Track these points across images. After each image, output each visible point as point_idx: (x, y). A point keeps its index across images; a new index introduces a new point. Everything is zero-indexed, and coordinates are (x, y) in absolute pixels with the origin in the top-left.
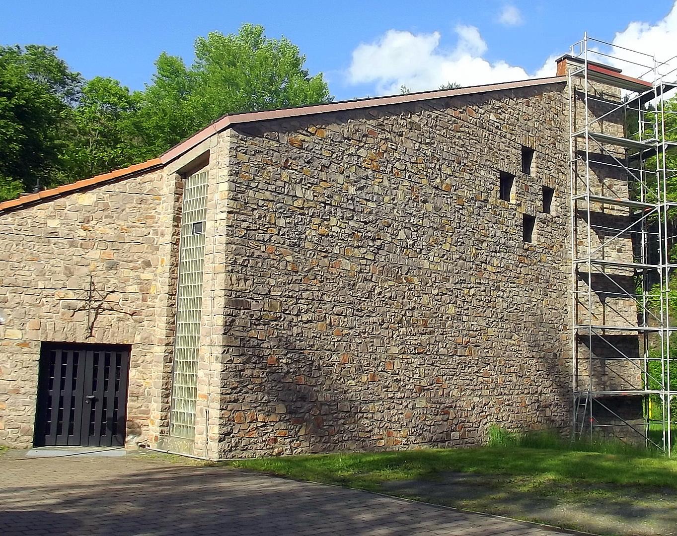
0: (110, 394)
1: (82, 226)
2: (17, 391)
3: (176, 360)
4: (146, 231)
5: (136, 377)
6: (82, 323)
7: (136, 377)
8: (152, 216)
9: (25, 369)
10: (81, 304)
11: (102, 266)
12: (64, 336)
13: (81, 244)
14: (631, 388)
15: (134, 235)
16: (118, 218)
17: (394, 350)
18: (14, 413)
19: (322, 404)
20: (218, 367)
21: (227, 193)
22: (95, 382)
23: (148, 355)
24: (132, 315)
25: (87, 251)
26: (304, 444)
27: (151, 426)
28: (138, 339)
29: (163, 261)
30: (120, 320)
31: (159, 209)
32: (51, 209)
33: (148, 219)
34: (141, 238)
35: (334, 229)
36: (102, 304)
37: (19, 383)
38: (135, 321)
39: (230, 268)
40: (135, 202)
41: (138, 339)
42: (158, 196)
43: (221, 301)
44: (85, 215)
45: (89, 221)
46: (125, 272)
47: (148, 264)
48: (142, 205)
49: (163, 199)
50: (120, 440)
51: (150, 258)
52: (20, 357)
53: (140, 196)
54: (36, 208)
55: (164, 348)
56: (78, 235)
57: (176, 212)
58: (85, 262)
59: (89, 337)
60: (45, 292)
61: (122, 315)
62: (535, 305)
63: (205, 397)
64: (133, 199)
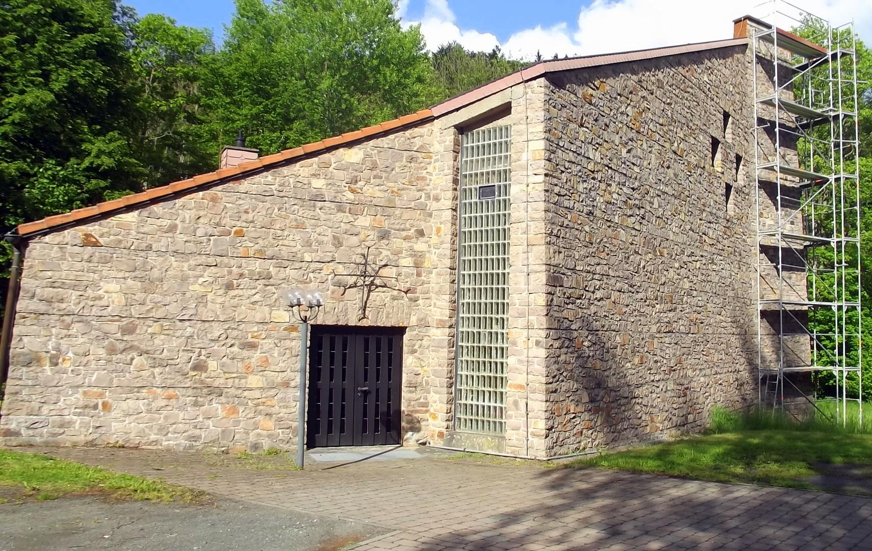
0: (383, 383)
1: (349, 187)
2: (286, 384)
3: (460, 344)
4: (418, 194)
5: (413, 365)
6: (354, 302)
7: (413, 365)
8: (423, 177)
9: (294, 358)
10: (351, 281)
11: (373, 235)
12: (335, 318)
13: (350, 209)
14: (803, 364)
15: (405, 198)
16: (387, 178)
18: (284, 410)
19: (611, 390)
20: (542, 353)
21: (543, 152)
22: (366, 371)
23: (426, 338)
24: (406, 293)
25: (356, 217)
26: (601, 435)
28: (414, 320)
29: (439, 230)
30: (394, 298)
31: (430, 168)
32: (315, 166)
33: (418, 181)
34: (413, 203)
36: (374, 280)
38: (410, 299)
39: (548, 239)
40: (404, 160)
41: (414, 320)
43: (543, 278)
44: (353, 175)
45: (356, 182)
46: (397, 242)
47: (421, 233)
48: (412, 164)
49: (434, 158)
50: (396, 437)
51: (423, 226)
54: (298, 164)
55: (447, 331)
56: (345, 198)
57: (455, 173)
58: (355, 231)
59: (362, 318)
60: (313, 266)
61: (395, 293)
64: (402, 157)
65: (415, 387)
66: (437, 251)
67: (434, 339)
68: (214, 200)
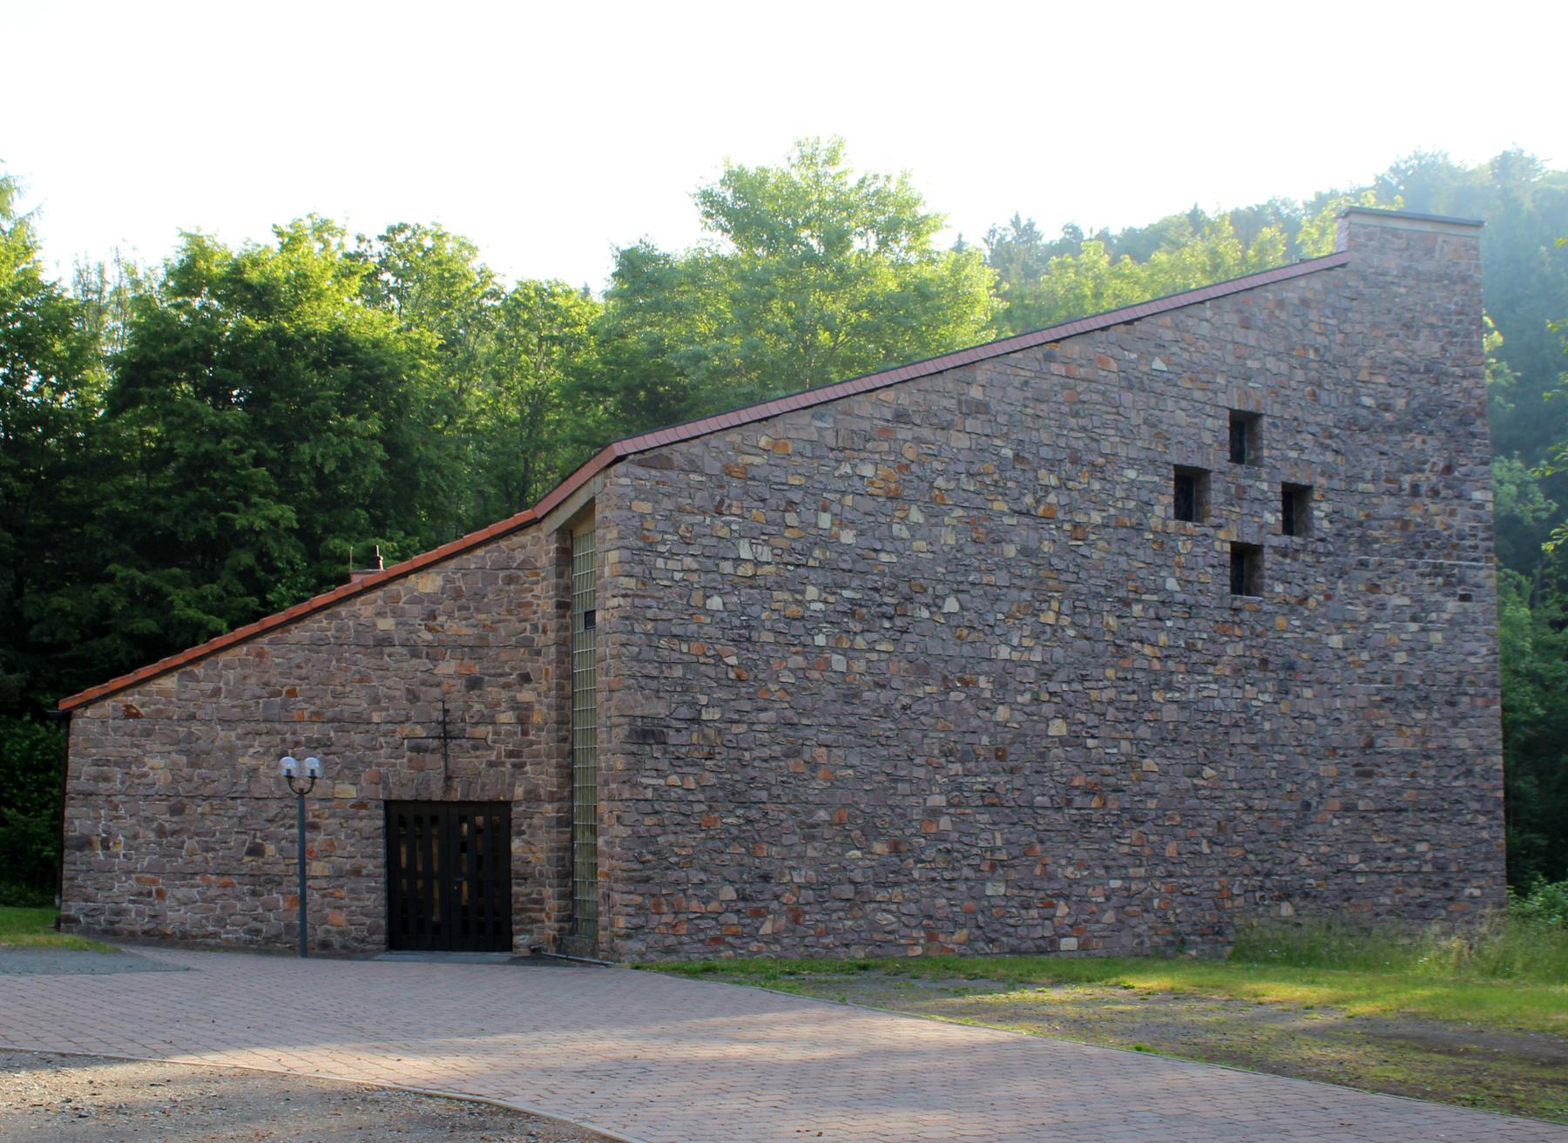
11: (460, 684)
13: (428, 653)
16: (477, 610)
17: (937, 800)
23: (537, 816)
27: (547, 923)
35: (814, 606)
37: (359, 861)
42: (535, 570)
46: (493, 692)
47: (526, 678)
52: (356, 823)
53: (508, 572)
58: (432, 680)
60: (383, 728)
62: (1256, 714)
63: (606, 875)
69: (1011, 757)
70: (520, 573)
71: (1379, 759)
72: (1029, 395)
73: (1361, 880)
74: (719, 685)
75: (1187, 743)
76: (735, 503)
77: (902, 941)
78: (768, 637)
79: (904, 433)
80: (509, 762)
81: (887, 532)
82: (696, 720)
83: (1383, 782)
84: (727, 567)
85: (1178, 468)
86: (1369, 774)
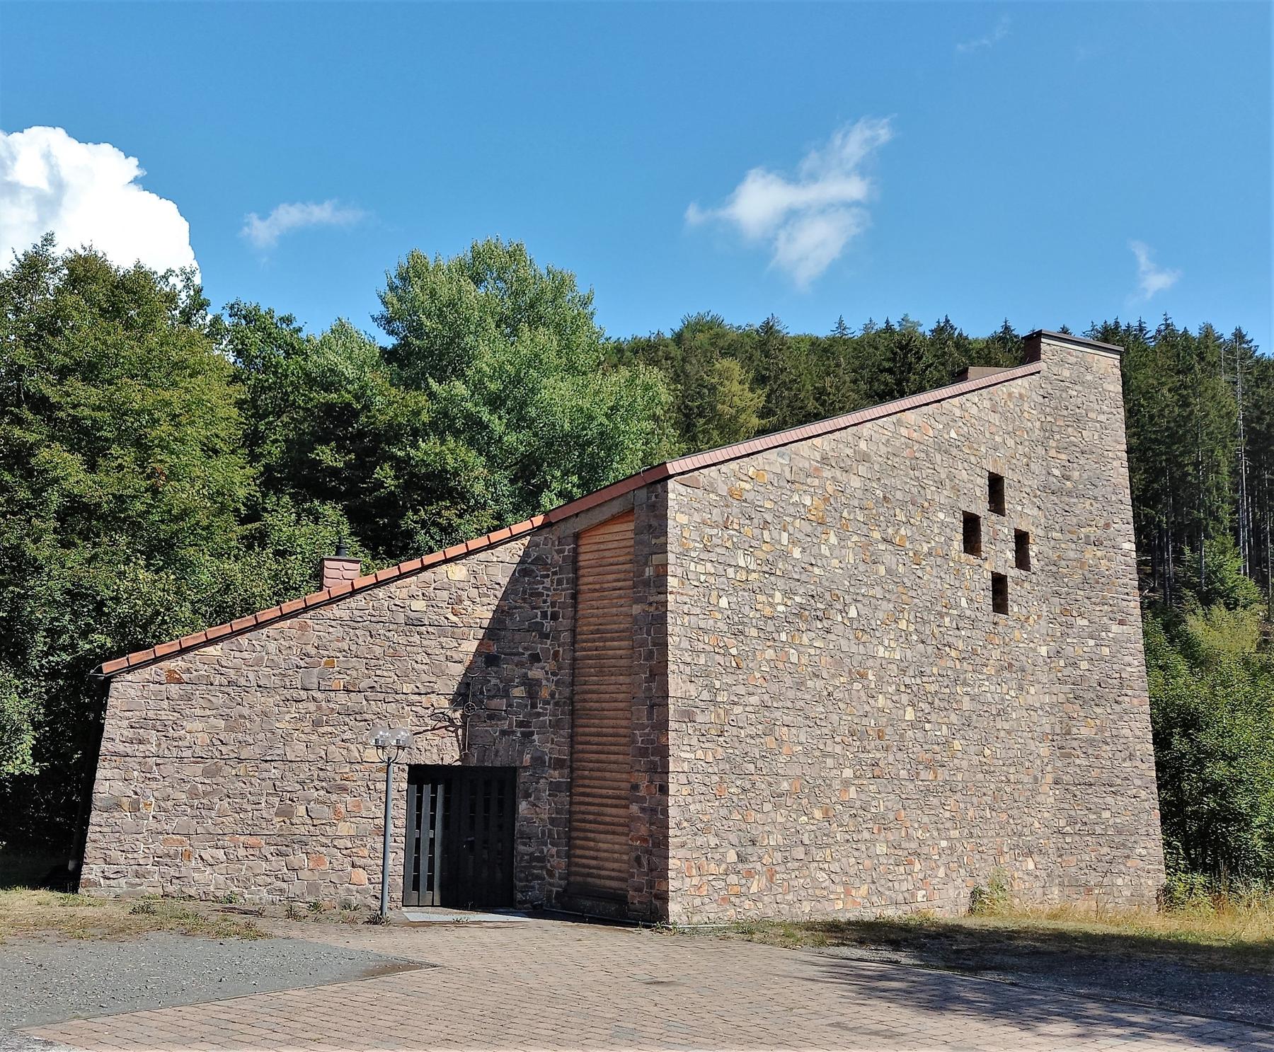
46: (507, 668)
47: (535, 658)
65: (530, 838)
66: (555, 679)
67: (551, 782)
68: (303, 628)
69: (887, 738)
70: (534, 568)
71: (1075, 744)
72: (890, 450)
73: (1068, 840)
74: (727, 672)
75: (975, 728)
76: (735, 520)
77: (832, 897)
78: (754, 632)
79: (827, 473)
80: (519, 731)
81: (818, 552)
82: (713, 702)
83: (1078, 761)
84: (731, 572)
85: (965, 513)
86: (1069, 756)
